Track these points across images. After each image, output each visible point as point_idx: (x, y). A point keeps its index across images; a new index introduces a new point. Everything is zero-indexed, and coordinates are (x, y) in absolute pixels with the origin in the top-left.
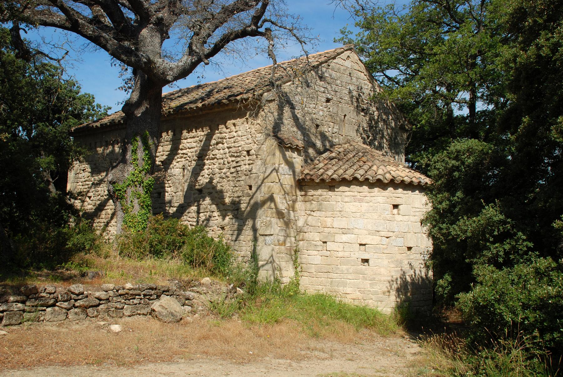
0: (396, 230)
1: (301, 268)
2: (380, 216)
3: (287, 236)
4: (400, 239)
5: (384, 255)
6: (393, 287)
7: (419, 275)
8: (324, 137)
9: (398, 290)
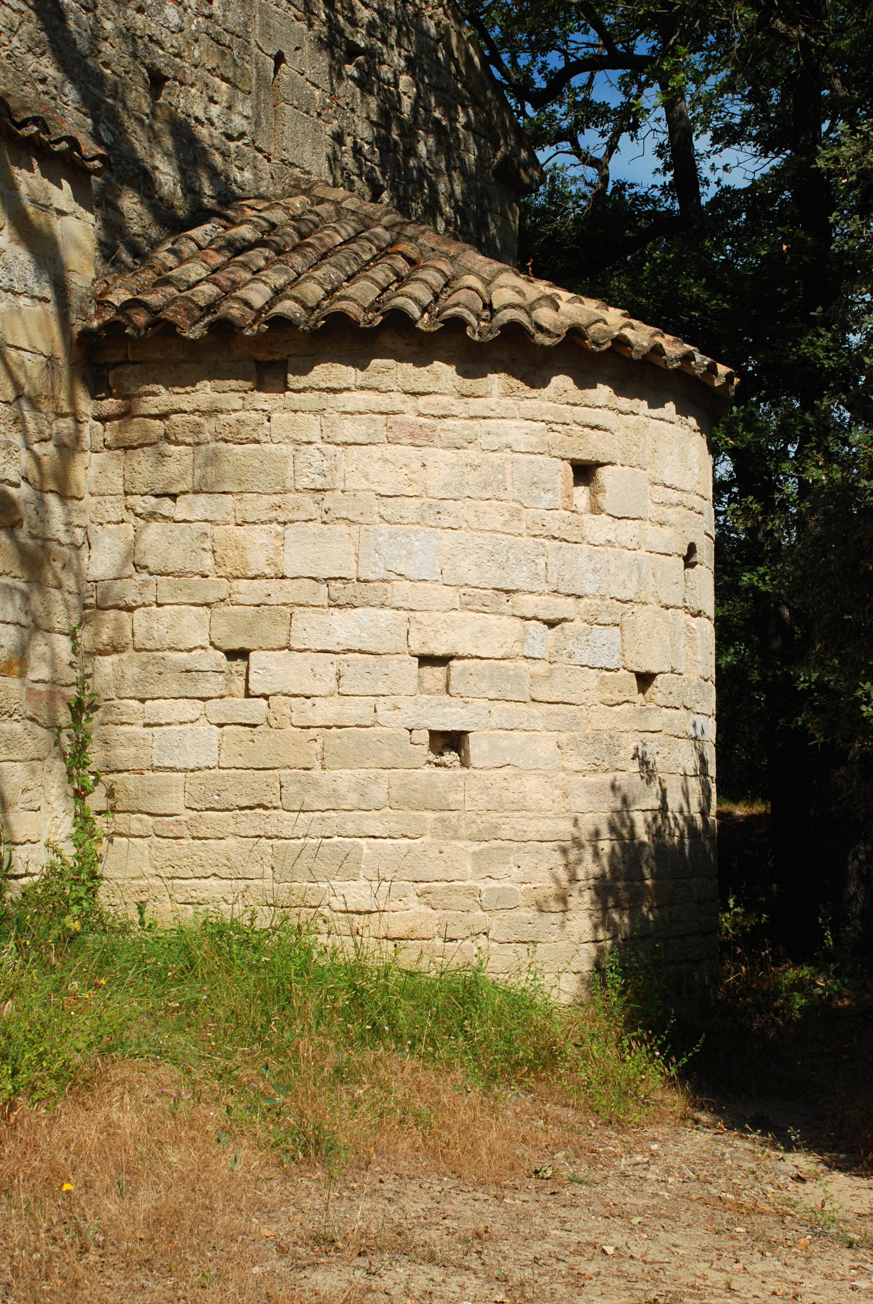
0: (588, 589)
1: (110, 794)
2: (515, 515)
3: (34, 626)
5: (536, 710)
8: (190, 152)
9: (603, 890)
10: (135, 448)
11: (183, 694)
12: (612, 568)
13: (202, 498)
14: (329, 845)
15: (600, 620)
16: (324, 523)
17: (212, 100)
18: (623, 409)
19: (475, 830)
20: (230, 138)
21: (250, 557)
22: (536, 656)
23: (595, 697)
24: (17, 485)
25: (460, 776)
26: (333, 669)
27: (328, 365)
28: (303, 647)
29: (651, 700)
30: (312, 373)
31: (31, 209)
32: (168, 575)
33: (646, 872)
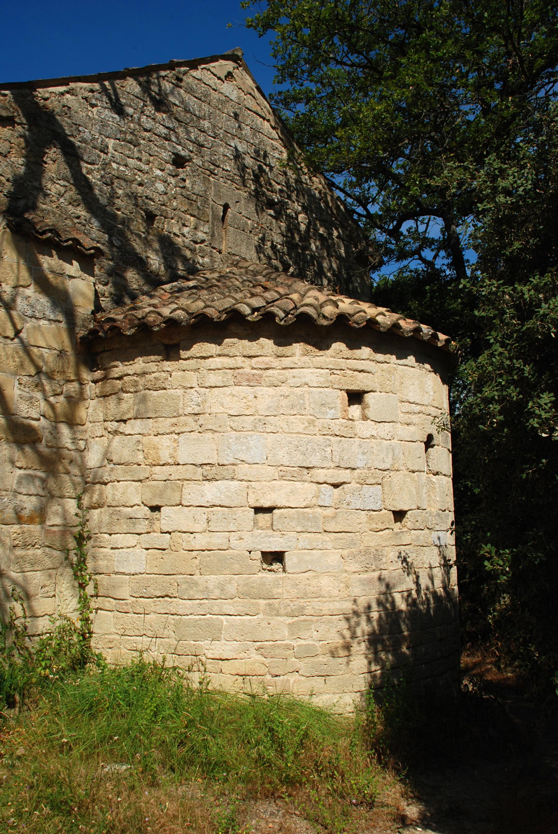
0: (359, 464)
2: (311, 423)
4: (372, 488)
5: (327, 537)
6: (359, 632)
7: (427, 589)
8: (168, 248)
9: (374, 641)
10: (108, 396)
11: (128, 531)
12: (375, 451)
13: (138, 422)
14: (204, 619)
15: (367, 482)
16: (199, 432)
17: (184, 225)
18: (379, 360)
19: (290, 611)
20: (196, 242)
21: (161, 453)
22: (326, 505)
23: (366, 527)
24: (38, 420)
25: (280, 578)
26: (205, 517)
27: (201, 344)
28: (188, 504)
29: (405, 526)
30: (193, 349)
31: (50, 276)
32: (122, 464)
33: (403, 627)
